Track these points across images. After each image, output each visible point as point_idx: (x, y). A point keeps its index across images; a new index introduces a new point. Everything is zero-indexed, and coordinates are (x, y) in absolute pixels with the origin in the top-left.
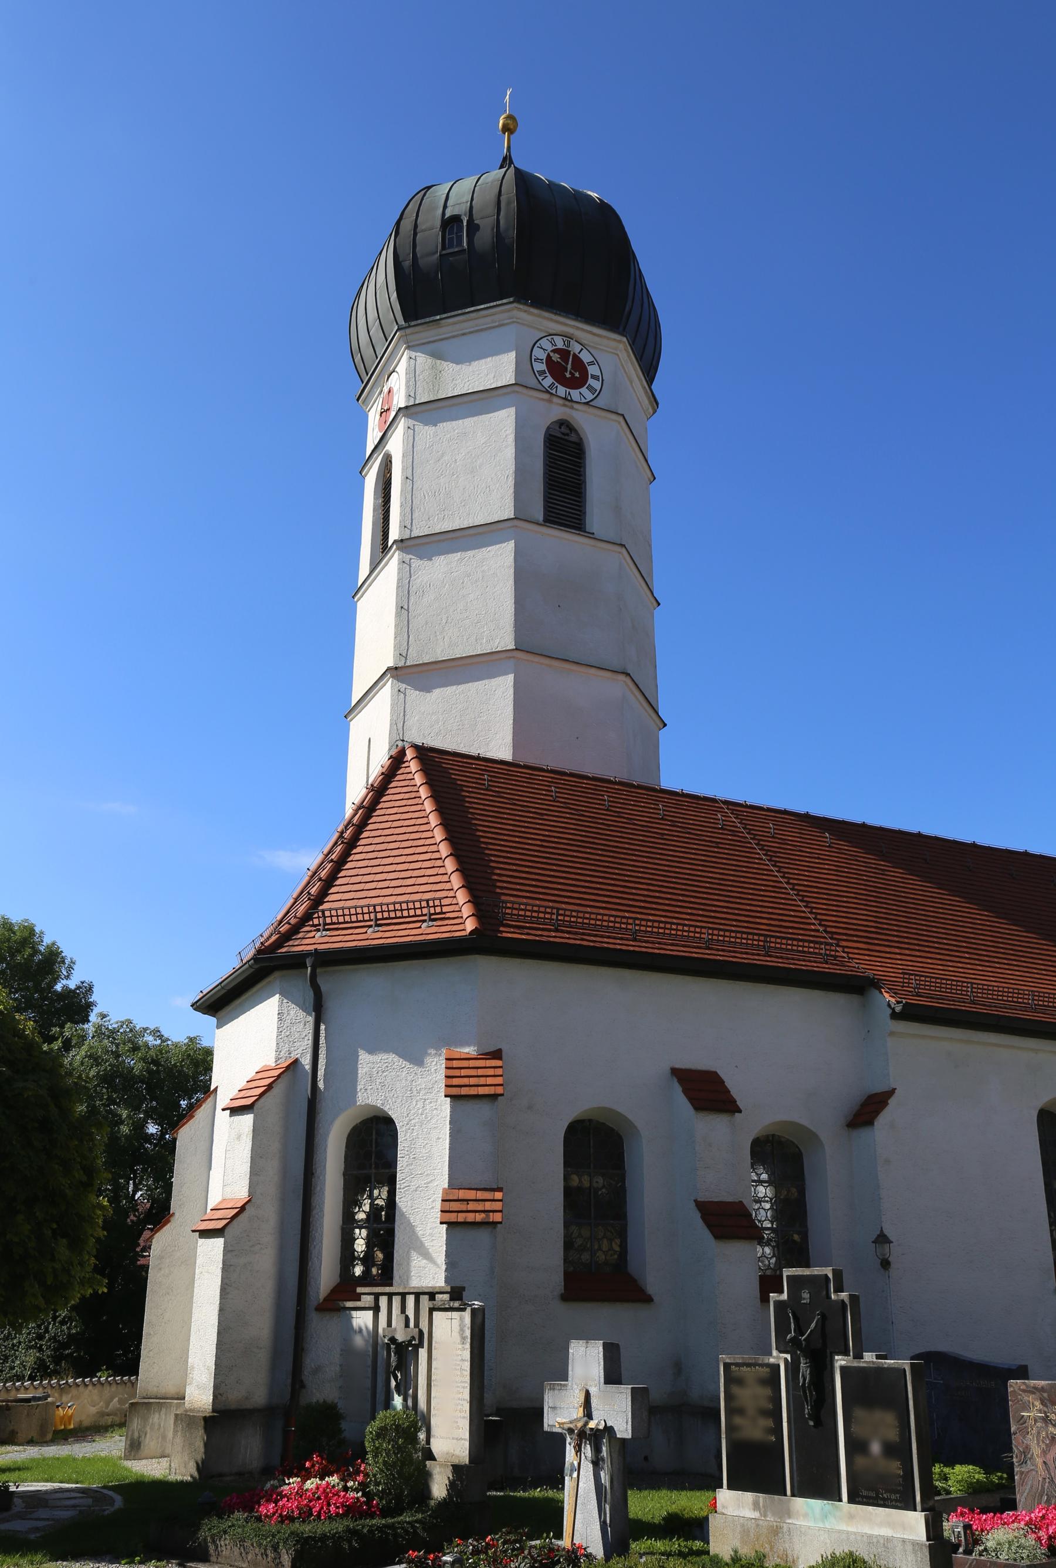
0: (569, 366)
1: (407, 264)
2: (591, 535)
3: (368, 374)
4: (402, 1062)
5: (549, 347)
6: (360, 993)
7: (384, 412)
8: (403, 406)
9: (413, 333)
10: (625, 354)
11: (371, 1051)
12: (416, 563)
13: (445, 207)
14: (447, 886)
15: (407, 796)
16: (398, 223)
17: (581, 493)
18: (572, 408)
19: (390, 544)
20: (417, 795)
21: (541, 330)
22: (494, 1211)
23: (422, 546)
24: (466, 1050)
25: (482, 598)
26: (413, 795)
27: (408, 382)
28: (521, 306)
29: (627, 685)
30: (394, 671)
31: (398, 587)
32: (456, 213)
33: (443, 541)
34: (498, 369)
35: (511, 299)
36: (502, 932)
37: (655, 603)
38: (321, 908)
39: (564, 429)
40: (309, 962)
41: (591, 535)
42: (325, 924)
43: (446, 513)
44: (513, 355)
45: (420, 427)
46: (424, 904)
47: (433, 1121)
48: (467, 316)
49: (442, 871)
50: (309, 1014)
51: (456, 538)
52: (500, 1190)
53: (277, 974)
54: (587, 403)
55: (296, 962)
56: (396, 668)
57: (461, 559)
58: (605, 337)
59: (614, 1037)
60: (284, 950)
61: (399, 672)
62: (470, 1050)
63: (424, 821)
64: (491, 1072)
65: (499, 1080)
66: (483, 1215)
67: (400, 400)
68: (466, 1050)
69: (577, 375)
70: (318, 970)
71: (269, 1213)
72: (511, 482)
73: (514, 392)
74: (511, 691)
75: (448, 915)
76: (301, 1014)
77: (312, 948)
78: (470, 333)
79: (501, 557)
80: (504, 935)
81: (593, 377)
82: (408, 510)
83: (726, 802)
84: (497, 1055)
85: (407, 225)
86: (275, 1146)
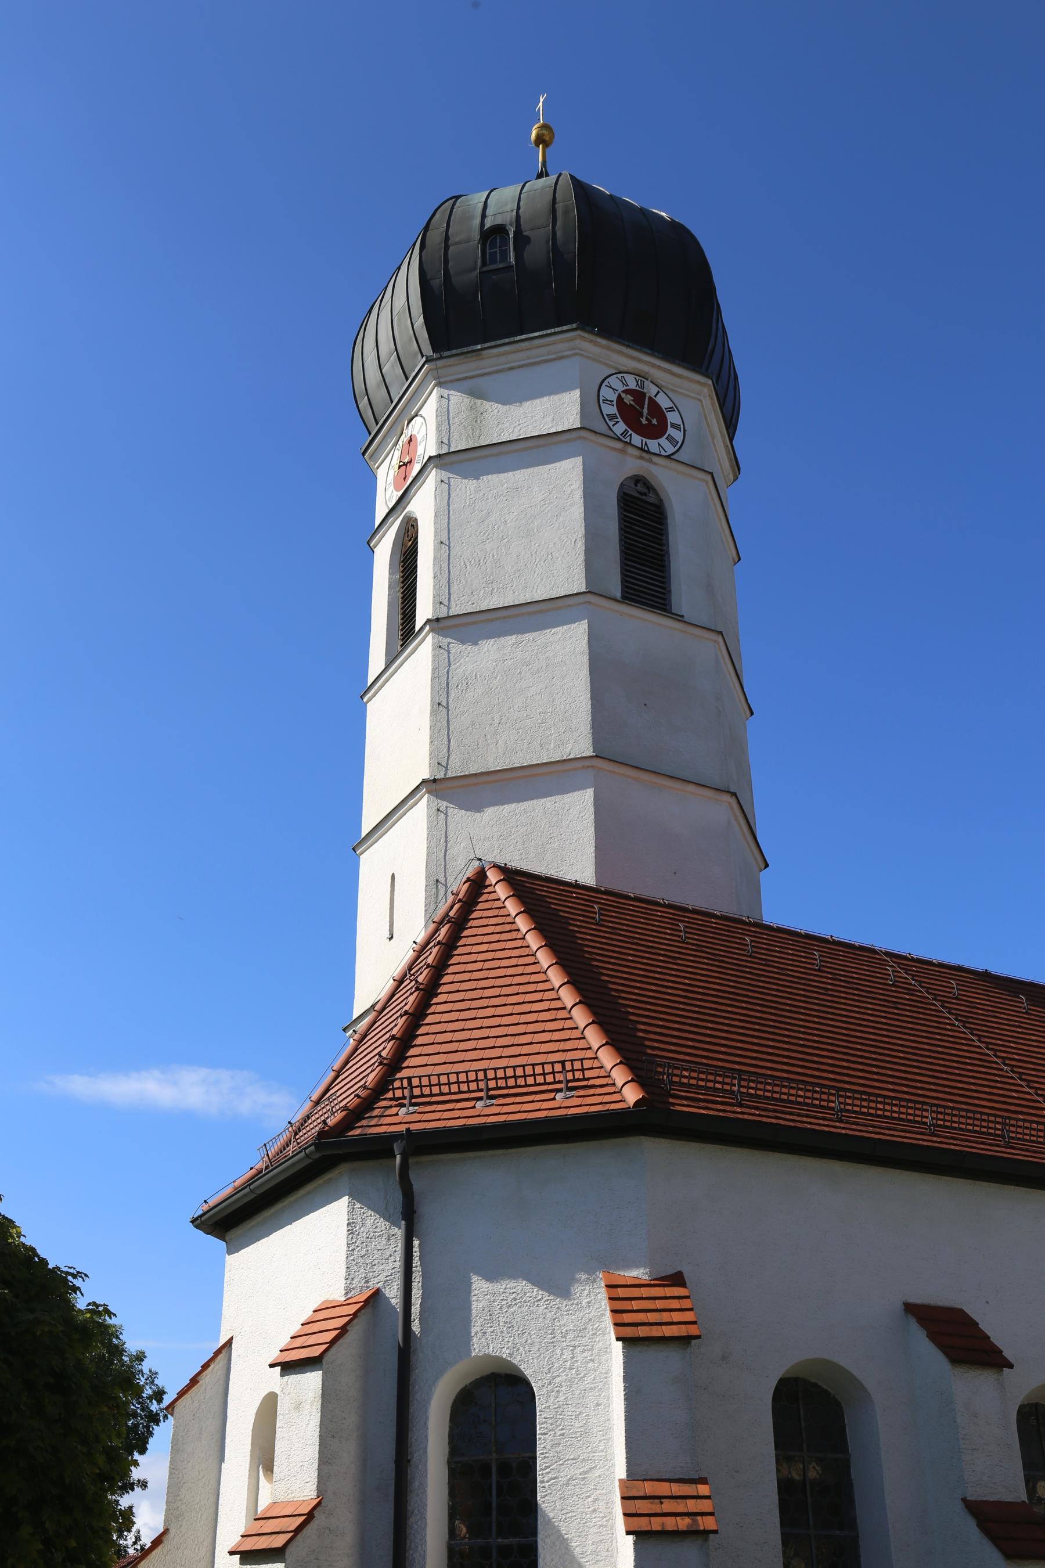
0: (645, 411)
1: (437, 282)
2: (679, 618)
3: (378, 423)
4: (536, 1292)
5: (621, 388)
6: (472, 1195)
7: (404, 465)
8: (433, 454)
9: (445, 367)
10: (709, 402)
11: (490, 1278)
12: (456, 648)
13: (484, 216)
14: (582, 1044)
15: (498, 929)
16: (426, 229)
17: (664, 566)
18: (651, 461)
19: (418, 626)
20: (514, 927)
21: (610, 366)
22: (702, 1514)
23: (458, 626)
24: (634, 1273)
25: (548, 691)
26: (508, 927)
27: (439, 426)
28: (586, 335)
29: (732, 808)
30: (432, 785)
31: (433, 679)
32: (499, 221)
33: (492, 620)
34: (561, 410)
35: (574, 326)
36: (674, 1104)
37: (748, 713)
38: (398, 1076)
39: (640, 487)
40: (397, 1148)
41: (679, 618)
42: (412, 1097)
43: (495, 585)
44: (576, 394)
45: (456, 481)
46: (558, 1067)
47: (589, 1379)
48: (517, 345)
49: (568, 1024)
50: (394, 1223)
51: (509, 617)
52: (703, 1481)
53: (344, 1167)
54: (669, 457)
55: (378, 1149)
56: (435, 781)
57: (517, 644)
58: (687, 378)
59: (835, 1255)
60: (357, 1132)
61: (437, 786)
62: (639, 1273)
63: (531, 960)
64: (675, 1304)
65: (688, 1316)
66: (687, 1520)
67: (428, 447)
68: (634, 1273)
69: (654, 422)
70: (411, 1161)
71: (344, 1520)
72: (580, 547)
73: (579, 438)
74: (591, 810)
75: (591, 1082)
76: (383, 1224)
77: (403, 1128)
78: (520, 367)
79: (569, 644)
80: (678, 1108)
81: (673, 426)
82: (445, 582)
83: (887, 954)
84: (677, 1279)
85: (436, 236)
86: (351, 1420)
